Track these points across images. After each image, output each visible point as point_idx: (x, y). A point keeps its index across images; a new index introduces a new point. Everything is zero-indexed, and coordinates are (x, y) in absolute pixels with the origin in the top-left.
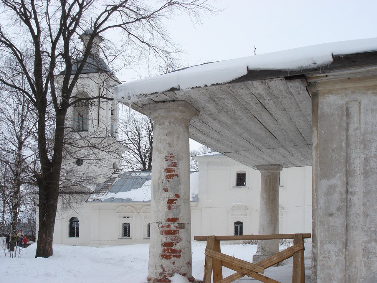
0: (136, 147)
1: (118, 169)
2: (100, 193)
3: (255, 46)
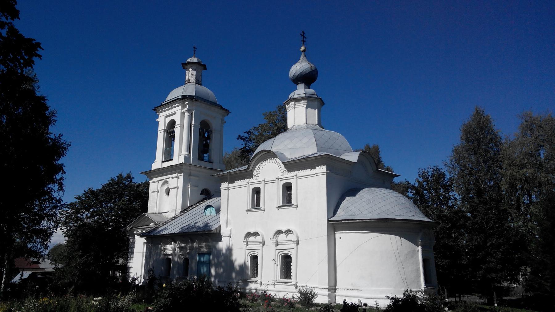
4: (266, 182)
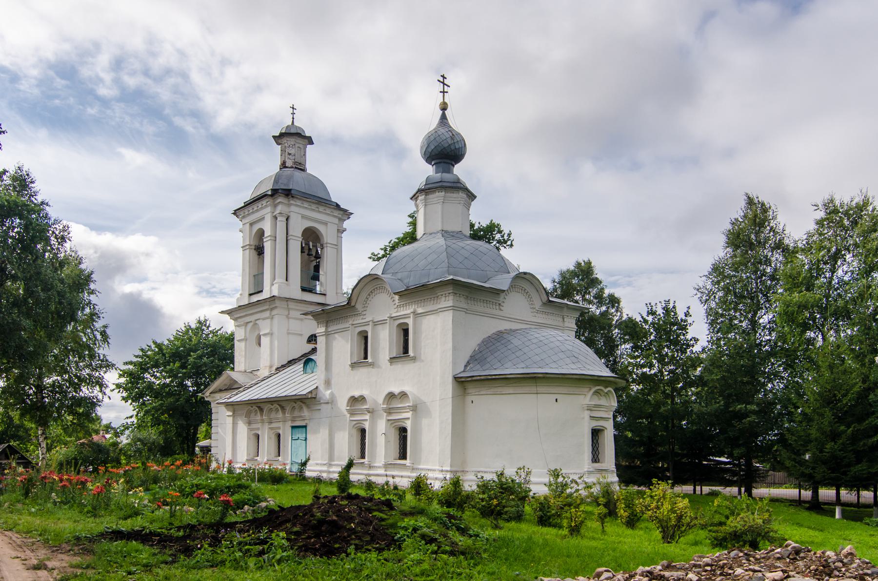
4: (376, 324)
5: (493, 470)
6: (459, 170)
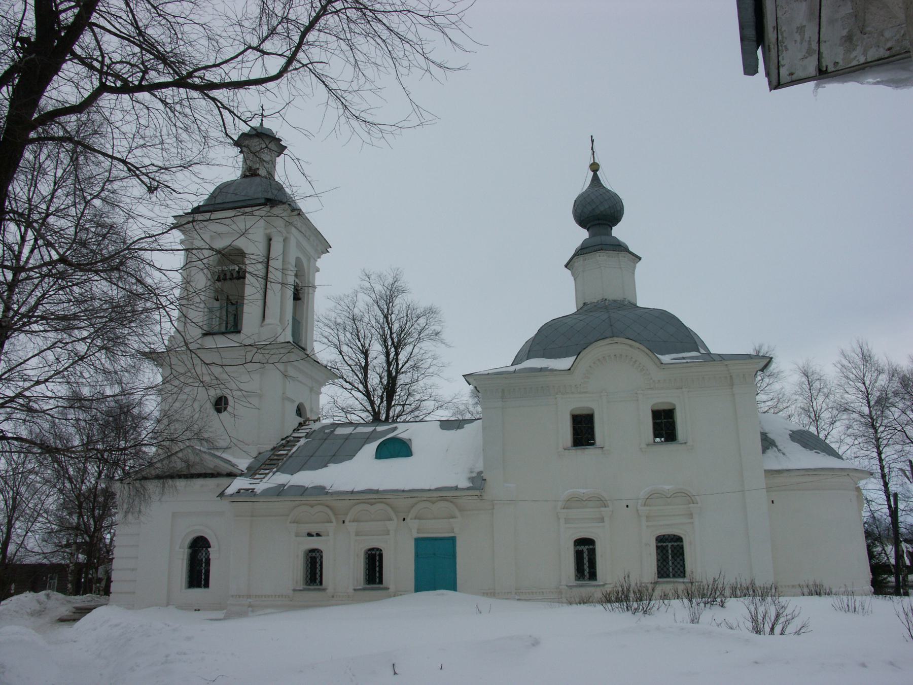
0: (357, 375)
1: (308, 420)
2: (256, 474)
3: (592, 136)
5: (789, 606)
6: (618, 232)
